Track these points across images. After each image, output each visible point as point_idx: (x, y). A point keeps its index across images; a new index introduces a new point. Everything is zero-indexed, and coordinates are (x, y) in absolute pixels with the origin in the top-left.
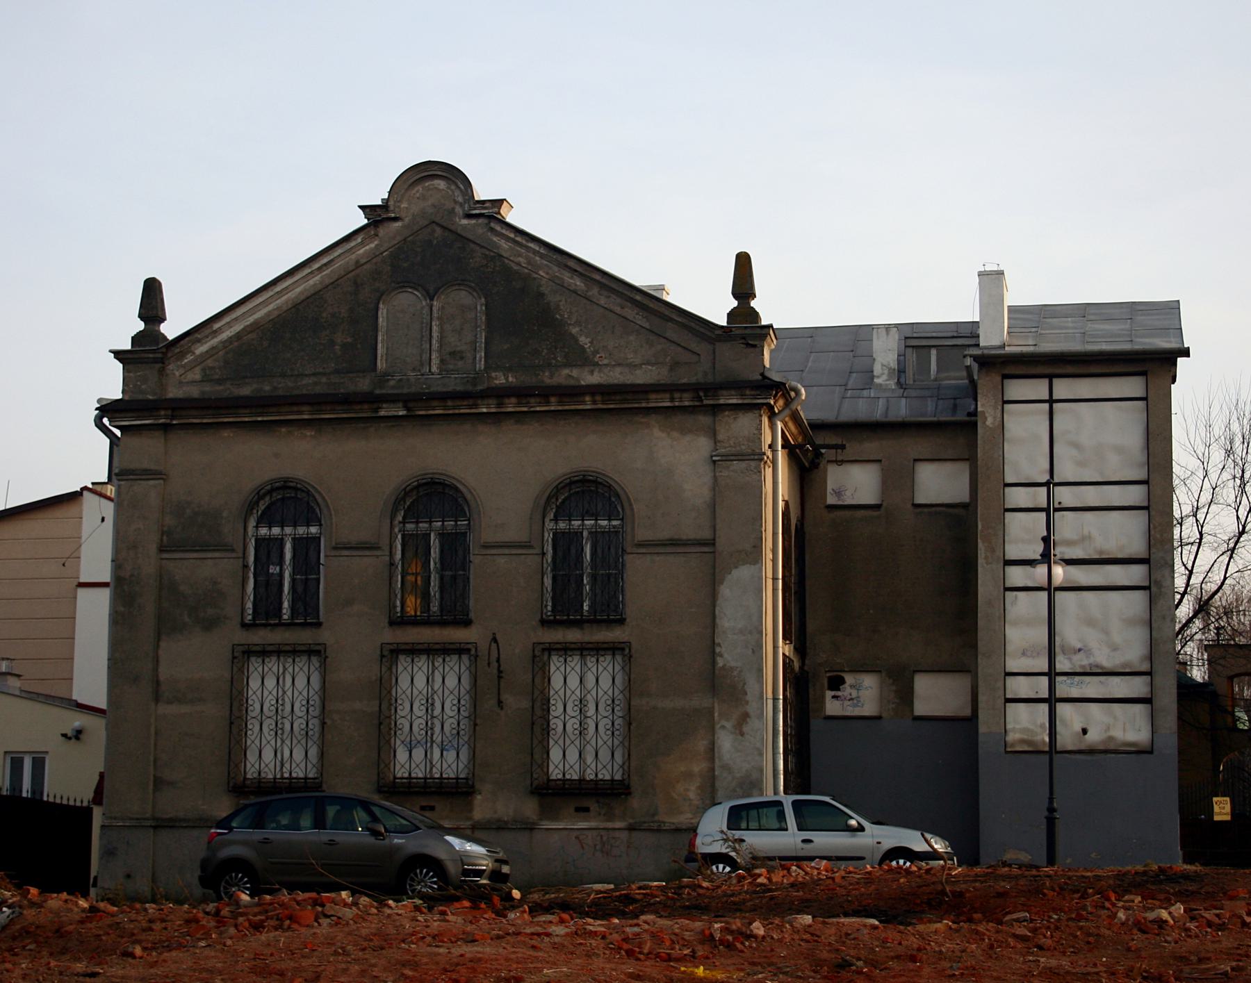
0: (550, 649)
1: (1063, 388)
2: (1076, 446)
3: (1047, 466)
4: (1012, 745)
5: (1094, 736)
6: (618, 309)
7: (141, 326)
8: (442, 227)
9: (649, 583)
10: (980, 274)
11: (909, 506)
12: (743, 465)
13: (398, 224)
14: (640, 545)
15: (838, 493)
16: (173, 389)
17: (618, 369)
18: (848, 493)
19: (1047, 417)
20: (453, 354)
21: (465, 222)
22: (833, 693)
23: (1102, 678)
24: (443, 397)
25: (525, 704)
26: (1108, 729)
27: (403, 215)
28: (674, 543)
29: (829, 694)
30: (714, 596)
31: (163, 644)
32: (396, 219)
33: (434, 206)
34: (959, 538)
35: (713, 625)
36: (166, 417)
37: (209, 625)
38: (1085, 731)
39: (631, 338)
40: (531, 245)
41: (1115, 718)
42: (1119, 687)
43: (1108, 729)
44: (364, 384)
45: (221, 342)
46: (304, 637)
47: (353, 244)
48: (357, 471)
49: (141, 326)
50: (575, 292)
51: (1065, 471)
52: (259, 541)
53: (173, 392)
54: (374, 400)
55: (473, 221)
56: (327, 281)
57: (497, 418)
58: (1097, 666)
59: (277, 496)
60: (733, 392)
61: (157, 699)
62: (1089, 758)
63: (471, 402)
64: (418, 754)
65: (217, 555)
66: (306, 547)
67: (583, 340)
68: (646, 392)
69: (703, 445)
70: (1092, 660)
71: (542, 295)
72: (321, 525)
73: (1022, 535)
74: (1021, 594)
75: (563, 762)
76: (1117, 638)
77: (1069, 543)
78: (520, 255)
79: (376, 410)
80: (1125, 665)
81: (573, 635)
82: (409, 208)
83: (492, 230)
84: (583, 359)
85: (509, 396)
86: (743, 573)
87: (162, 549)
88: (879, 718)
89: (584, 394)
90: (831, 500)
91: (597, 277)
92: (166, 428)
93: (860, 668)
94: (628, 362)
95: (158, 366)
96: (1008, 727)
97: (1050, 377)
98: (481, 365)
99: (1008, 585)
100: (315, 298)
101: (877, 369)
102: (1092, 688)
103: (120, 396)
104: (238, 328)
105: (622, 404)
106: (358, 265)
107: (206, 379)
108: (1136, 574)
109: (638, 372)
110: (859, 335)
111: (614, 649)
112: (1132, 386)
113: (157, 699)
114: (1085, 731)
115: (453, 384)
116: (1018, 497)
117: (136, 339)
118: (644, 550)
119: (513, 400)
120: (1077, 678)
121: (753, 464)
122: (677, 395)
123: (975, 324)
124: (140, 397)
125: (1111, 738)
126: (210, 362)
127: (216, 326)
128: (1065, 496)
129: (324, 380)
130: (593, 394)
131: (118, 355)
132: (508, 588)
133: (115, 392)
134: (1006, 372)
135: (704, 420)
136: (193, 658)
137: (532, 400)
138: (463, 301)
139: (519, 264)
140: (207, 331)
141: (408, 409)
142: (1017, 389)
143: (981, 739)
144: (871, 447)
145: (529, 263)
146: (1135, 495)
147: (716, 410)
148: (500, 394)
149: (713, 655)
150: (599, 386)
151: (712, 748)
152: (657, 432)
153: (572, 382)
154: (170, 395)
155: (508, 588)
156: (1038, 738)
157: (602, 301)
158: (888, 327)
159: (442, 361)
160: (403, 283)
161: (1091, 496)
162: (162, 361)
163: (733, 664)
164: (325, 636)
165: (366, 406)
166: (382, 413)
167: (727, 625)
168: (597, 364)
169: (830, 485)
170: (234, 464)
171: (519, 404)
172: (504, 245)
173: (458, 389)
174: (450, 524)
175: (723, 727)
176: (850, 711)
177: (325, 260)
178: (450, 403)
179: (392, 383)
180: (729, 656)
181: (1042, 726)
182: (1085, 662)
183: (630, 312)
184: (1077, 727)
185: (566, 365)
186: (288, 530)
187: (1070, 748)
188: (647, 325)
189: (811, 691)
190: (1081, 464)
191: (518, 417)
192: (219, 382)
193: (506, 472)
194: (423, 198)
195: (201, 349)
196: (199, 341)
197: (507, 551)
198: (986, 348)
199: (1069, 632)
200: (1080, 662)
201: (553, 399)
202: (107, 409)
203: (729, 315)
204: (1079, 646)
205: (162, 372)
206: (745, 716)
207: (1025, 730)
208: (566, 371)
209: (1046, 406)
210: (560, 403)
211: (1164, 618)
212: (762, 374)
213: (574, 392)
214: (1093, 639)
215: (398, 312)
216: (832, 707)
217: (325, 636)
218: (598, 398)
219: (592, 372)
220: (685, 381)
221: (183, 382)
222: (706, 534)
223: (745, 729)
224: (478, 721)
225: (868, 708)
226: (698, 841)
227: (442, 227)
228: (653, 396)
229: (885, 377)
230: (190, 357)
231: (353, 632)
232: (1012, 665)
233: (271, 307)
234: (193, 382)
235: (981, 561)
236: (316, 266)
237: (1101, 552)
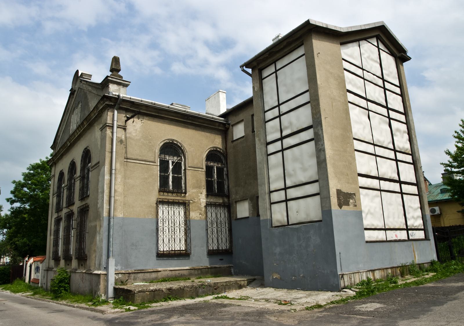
88: (248, 217)
146: (306, 98)
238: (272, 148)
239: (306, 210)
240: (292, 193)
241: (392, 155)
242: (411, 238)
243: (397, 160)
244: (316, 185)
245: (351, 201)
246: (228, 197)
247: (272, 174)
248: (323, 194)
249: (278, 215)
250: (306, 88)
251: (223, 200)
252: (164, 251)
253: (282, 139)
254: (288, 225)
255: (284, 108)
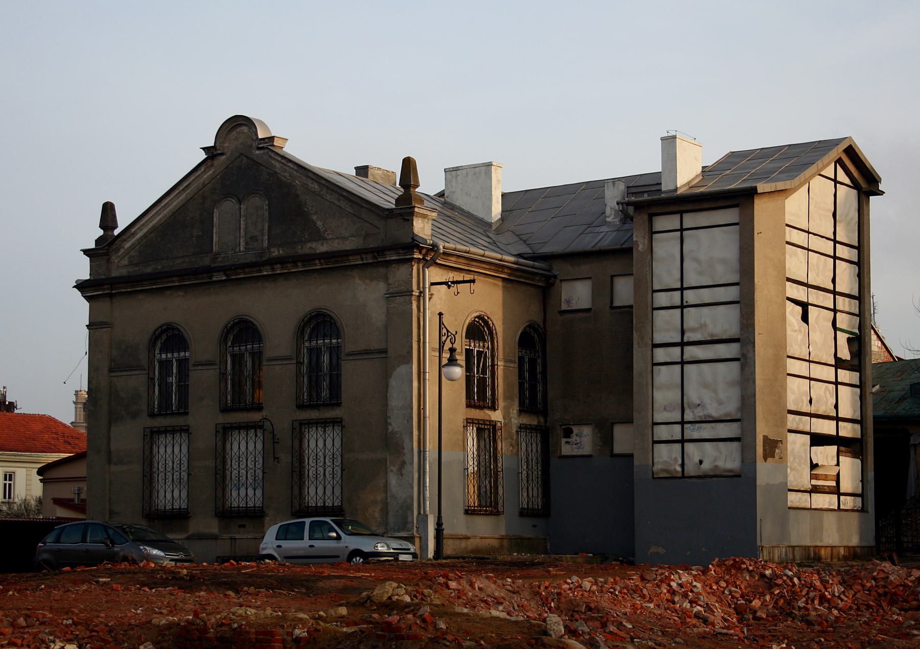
0: (310, 423)
1: (690, 220)
2: (697, 260)
3: (678, 276)
4: (657, 473)
5: (706, 466)
6: (337, 202)
7: (101, 232)
8: (247, 157)
9: (355, 377)
10: (663, 139)
11: (608, 308)
12: (402, 299)
13: (224, 157)
14: (348, 355)
15: (568, 302)
16: (131, 268)
17: (337, 241)
18: (574, 301)
19: (679, 241)
20: (251, 238)
21: (258, 152)
22: (566, 440)
23: (713, 425)
24: (244, 266)
25: (290, 459)
26: (715, 460)
27: (226, 151)
28: (367, 352)
29: (564, 440)
30: (387, 386)
31: (112, 429)
32: (222, 154)
33: (242, 144)
34: (621, 330)
35: (387, 405)
36: (108, 289)
37: (135, 415)
38: (701, 462)
39: (344, 220)
40: (290, 164)
41: (720, 452)
42: (724, 430)
43: (715, 460)
44: (206, 261)
45: (138, 240)
46: (179, 421)
47: (199, 172)
48: (201, 315)
49: (101, 232)
50: (314, 192)
51: (691, 279)
52: (161, 362)
53: (115, 273)
54: (209, 271)
55: (262, 152)
56: (189, 197)
57: (274, 277)
58: (709, 416)
59: (164, 337)
60: (392, 252)
61: (110, 462)
62: (700, 481)
63: (257, 269)
64: (243, 492)
65: (137, 372)
66: (182, 363)
67: (319, 223)
68: (347, 256)
69: (380, 288)
70: (705, 412)
71: (297, 196)
72: (612, 307)
73: (665, 325)
74: (663, 368)
75: (314, 495)
76: (722, 396)
77: (693, 330)
78: (285, 171)
79: (211, 277)
80: (726, 415)
81: (314, 414)
82: (229, 146)
83: (270, 157)
84: (318, 236)
85: (276, 264)
86: (402, 369)
87: (111, 370)
88: (590, 456)
89: (314, 260)
90: (564, 307)
91: (324, 182)
92: (111, 296)
93: (581, 423)
94: (340, 236)
95: (106, 257)
96: (655, 460)
97: (681, 213)
98: (266, 244)
99: (655, 362)
100: (183, 208)
101: (608, 211)
102: (706, 431)
103: (88, 278)
104: (145, 230)
105: (337, 264)
106: (204, 185)
107: (131, 264)
108: (731, 350)
109: (347, 242)
110: (595, 188)
111: (336, 422)
112: (731, 215)
113: (110, 462)
114: (701, 462)
115: (250, 258)
116: (662, 299)
117: (98, 241)
118: (351, 358)
119: (279, 266)
120: (697, 425)
121: (407, 298)
122: (364, 256)
123: (658, 174)
124: (99, 277)
125: (716, 467)
126: (132, 253)
127: (133, 230)
128: (691, 297)
129: (187, 260)
130: (319, 259)
131: (86, 252)
132: (279, 385)
133: (86, 276)
134: (652, 211)
135: (382, 270)
136: (127, 436)
137: (289, 265)
138: (258, 203)
139: (285, 177)
140: (128, 234)
141: (227, 276)
142: (661, 223)
143: (635, 470)
144: (586, 268)
145: (291, 176)
146: (732, 293)
147: (388, 263)
148: (272, 262)
149: (386, 424)
150: (327, 253)
151: (386, 485)
152: (357, 281)
153: (312, 252)
154: (113, 275)
155: (279, 385)
156: (672, 468)
157: (328, 197)
158: (614, 181)
159: (247, 243)
160: (226, 195)
161: (706, 296)
162: (107, 254)
163: (396, 429)
164: (190, 420)
165: (205, 275)
166: (214, 279)
167: (393, 404)
168: (326, 239)
169: (563, 297)
170: (146, 314)
171: (282, 268)
172: (278, 165)
173: (254, 260)
174: (182, 354)
175: (392, 471)
176: (576, 452)
177: (186, 184)
178: (247, 270)
179: (220, 259)
180: (395, 425)
181: (676, 459)
182: (701, 414)
183: (343, 204)
184: (697, 460)
185: (309, 241)
186: (176, 355)
187: (692, 474)
188: (351, 211)
189: (551, 439)
190: (700, 273)
191: (286, 276)
192: (137, 265)
193: (277, 309)
194: (236, 139)
195: (127, 245)
196: (125, 240)
197: (280, 362)
198: (665, 192)
199: (693, 394)
200: (699, 413)
201: (299, 264)
202: (81, 286)
203: (732, 155)
204: (698, 402)
205: (108, 261)
206: (403, 463)
207: (666, 462)
208: (309, 245)
209: (679, 233)
210: (304, 266)
211: (748, 380)
212: (413, 238)
213: (308, 259)
214: (707, 397)
215: (224, 213)
216: (566, 450)
217: (190, 420)
218: (322, 261)
219: (322, 244)
220: (372, 246)
221: (120, 266)
222: (382, 346)
223: (404, 472)
224: (266, 471)
225: (587, 449)
226: (262, 546)
227: (247, 157)
228: (351, 258)
229: (612, 217)
230: (122, 251)
231: (204, 417)
232: (658, 418)
233: (161, 216)
234: (124, 266)
235: (635, 346)
236: (181, 188)
237: (712, 335)
238: (661, 355)
239: (726, 458)
240: (692, 432)
241: (828, 247)
242: (842, 507)
243: (835, 258)
244: (735, 425)
245: (777, 451)
246: (544, 413)
247: (659, 396)
248: (744, 440)
249: (666, 457)
250: (735, 278)
251: (539, 422)
252: (239, 507)
253: (682, 344)
254: (683, 477)
255: (691, 297)
